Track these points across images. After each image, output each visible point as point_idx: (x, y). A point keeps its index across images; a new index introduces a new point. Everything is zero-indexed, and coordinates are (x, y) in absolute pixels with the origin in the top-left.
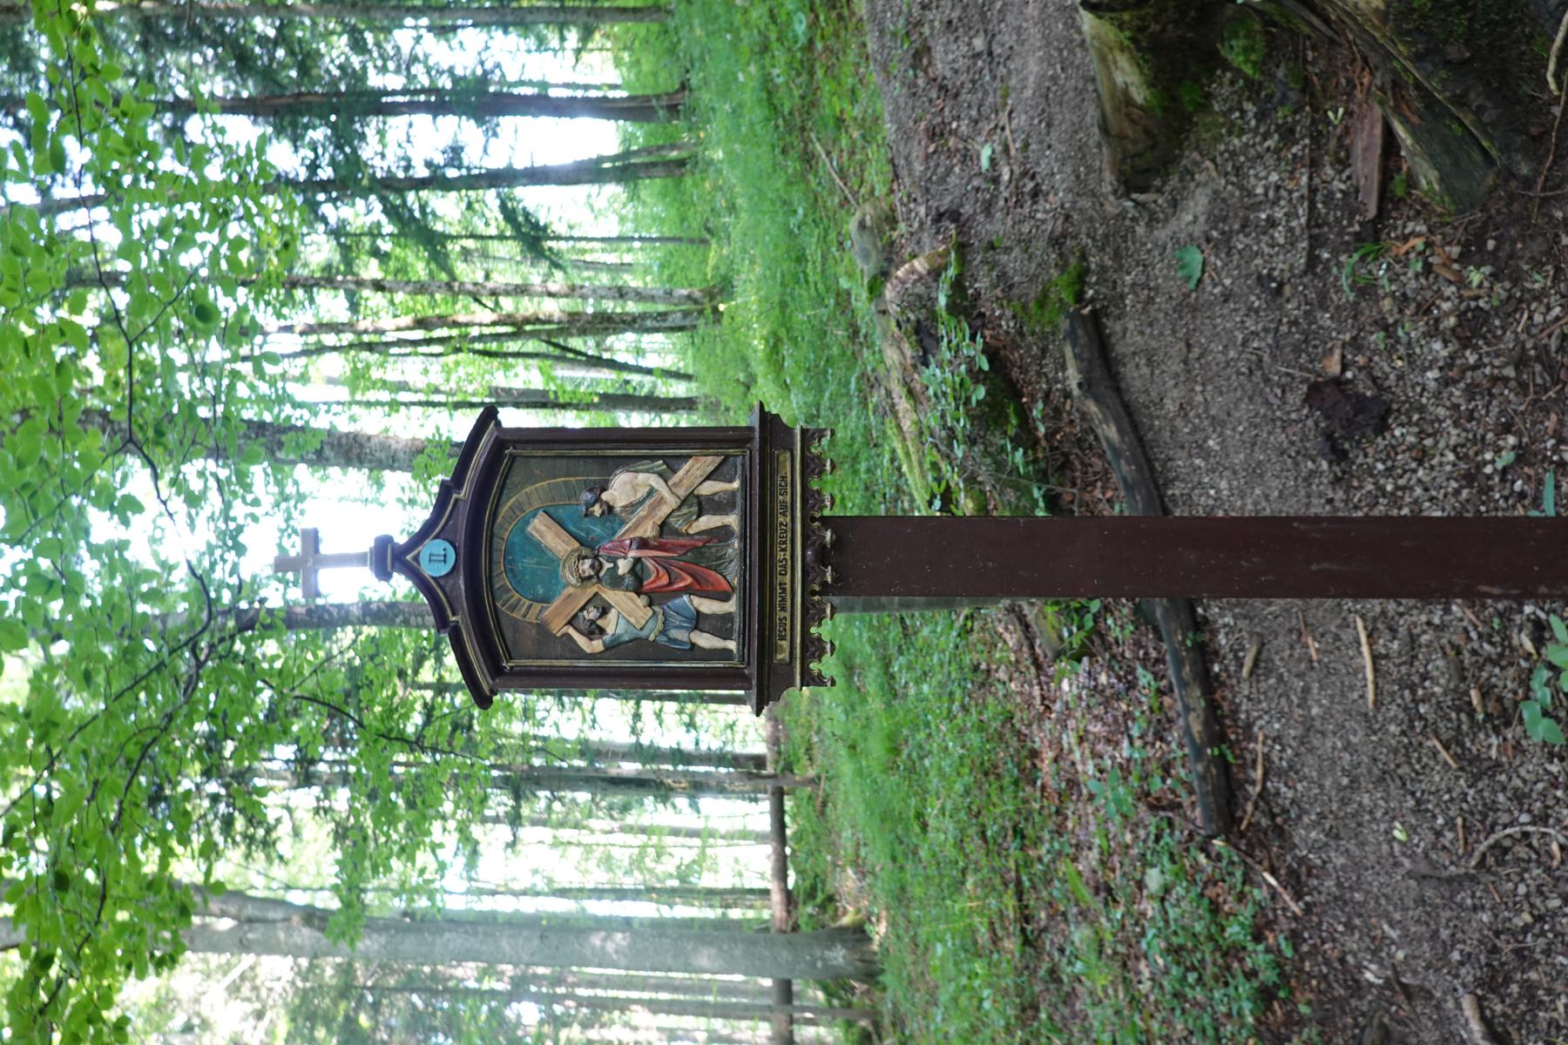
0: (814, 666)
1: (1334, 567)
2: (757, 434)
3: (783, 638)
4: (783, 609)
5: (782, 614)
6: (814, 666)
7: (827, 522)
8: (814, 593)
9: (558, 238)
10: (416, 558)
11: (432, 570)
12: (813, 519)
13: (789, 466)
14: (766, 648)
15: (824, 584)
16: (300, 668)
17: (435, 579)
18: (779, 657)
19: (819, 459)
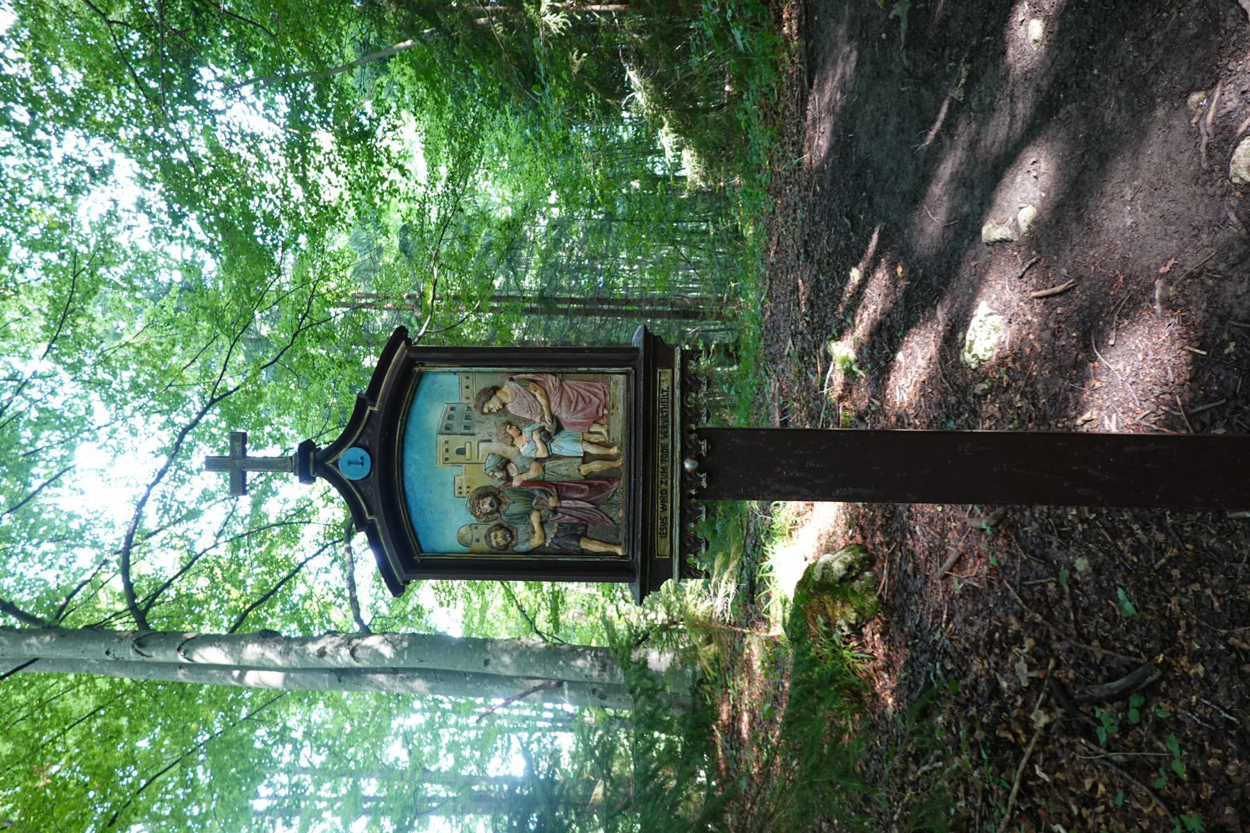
0: (691, 559)
1: (875, 236)
2: (642, 353)
3: (664, 536)
4: (664, 509)
5: (663, 515)
6: (691, 559)
7: (702, 433)
8: (691, 496)
9: (536, 689)
10: (336, 464)
11: (348, 474)
12: (691, 431)
13: (668, 379)
14: (648, 546)
15: (700, 488)
16: (363, 73)
17: (352, 481)
18: (699, 779)
19: (697, 408)
